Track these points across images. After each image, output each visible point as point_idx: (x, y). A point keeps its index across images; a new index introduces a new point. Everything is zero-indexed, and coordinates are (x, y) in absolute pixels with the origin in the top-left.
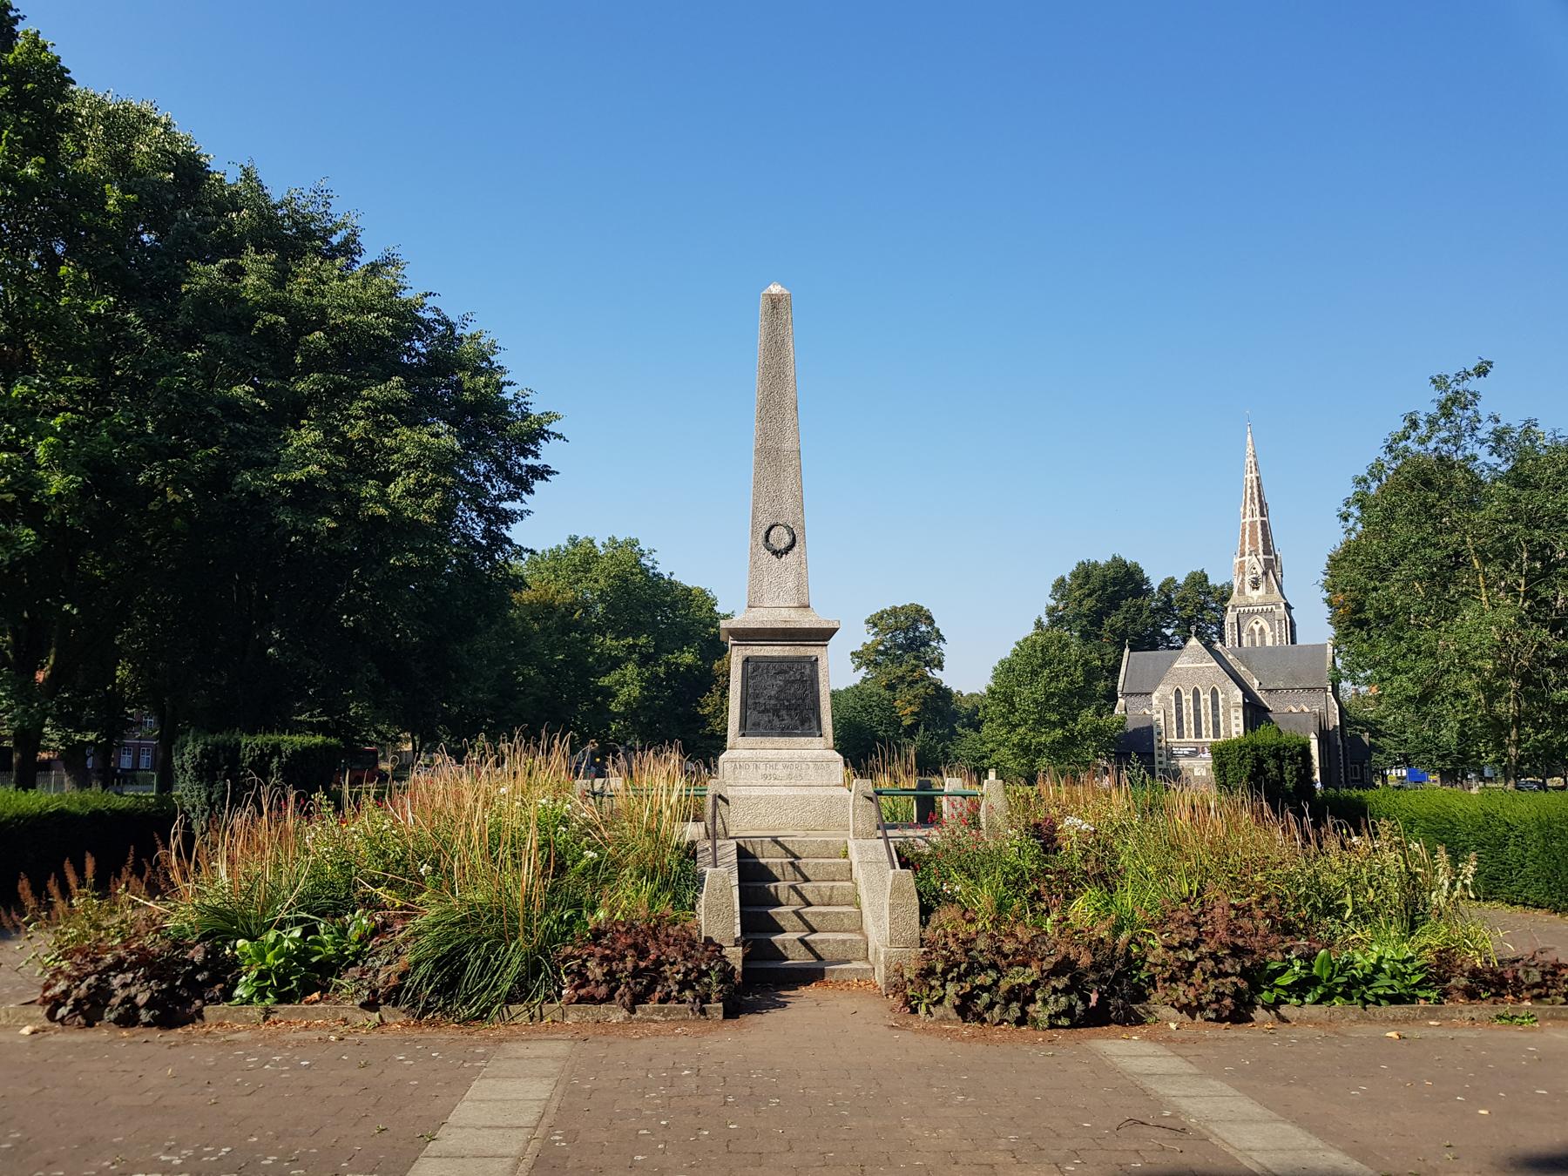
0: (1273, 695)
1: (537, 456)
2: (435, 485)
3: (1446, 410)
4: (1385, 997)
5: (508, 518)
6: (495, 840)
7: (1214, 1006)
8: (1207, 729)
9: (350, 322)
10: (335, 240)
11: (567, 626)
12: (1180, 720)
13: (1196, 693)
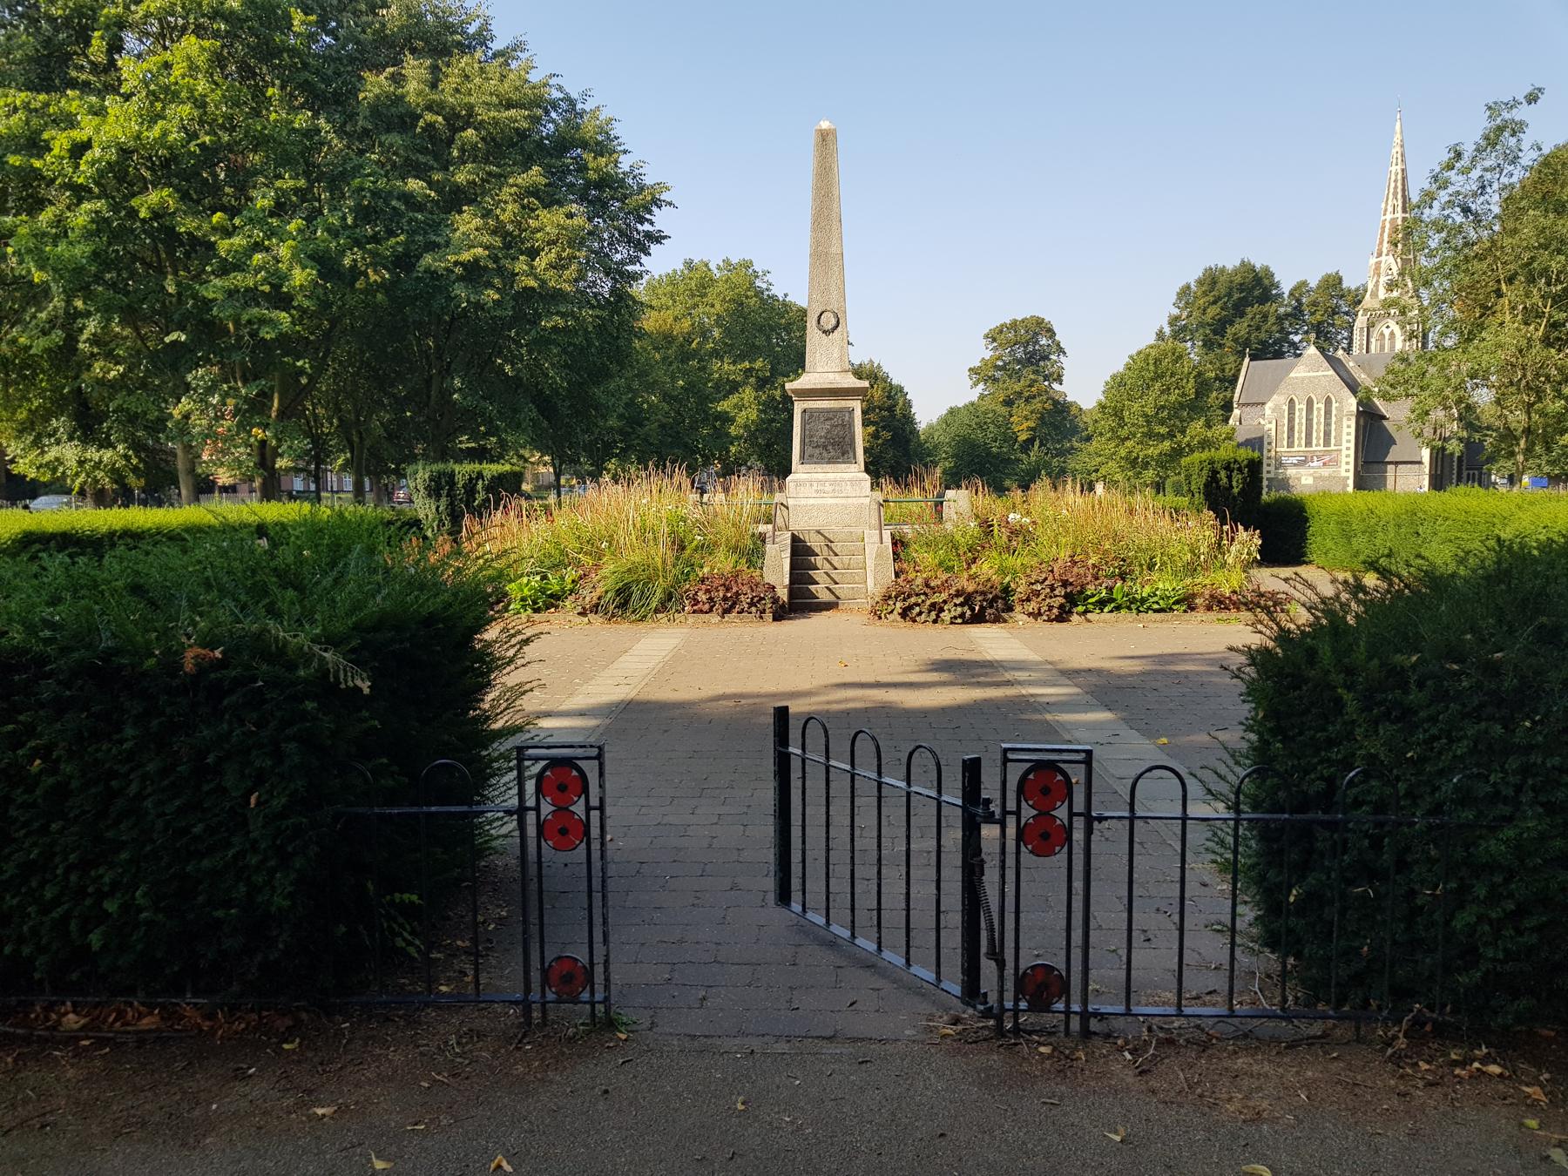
1: (652, 223)
2: (572, 257)
3: (1491, 140)
6: (643, 530)
8: (1318, 438)
10: (472, 30)
11: (685, 356)
12: (1291, 429)
13: (1310, 403)
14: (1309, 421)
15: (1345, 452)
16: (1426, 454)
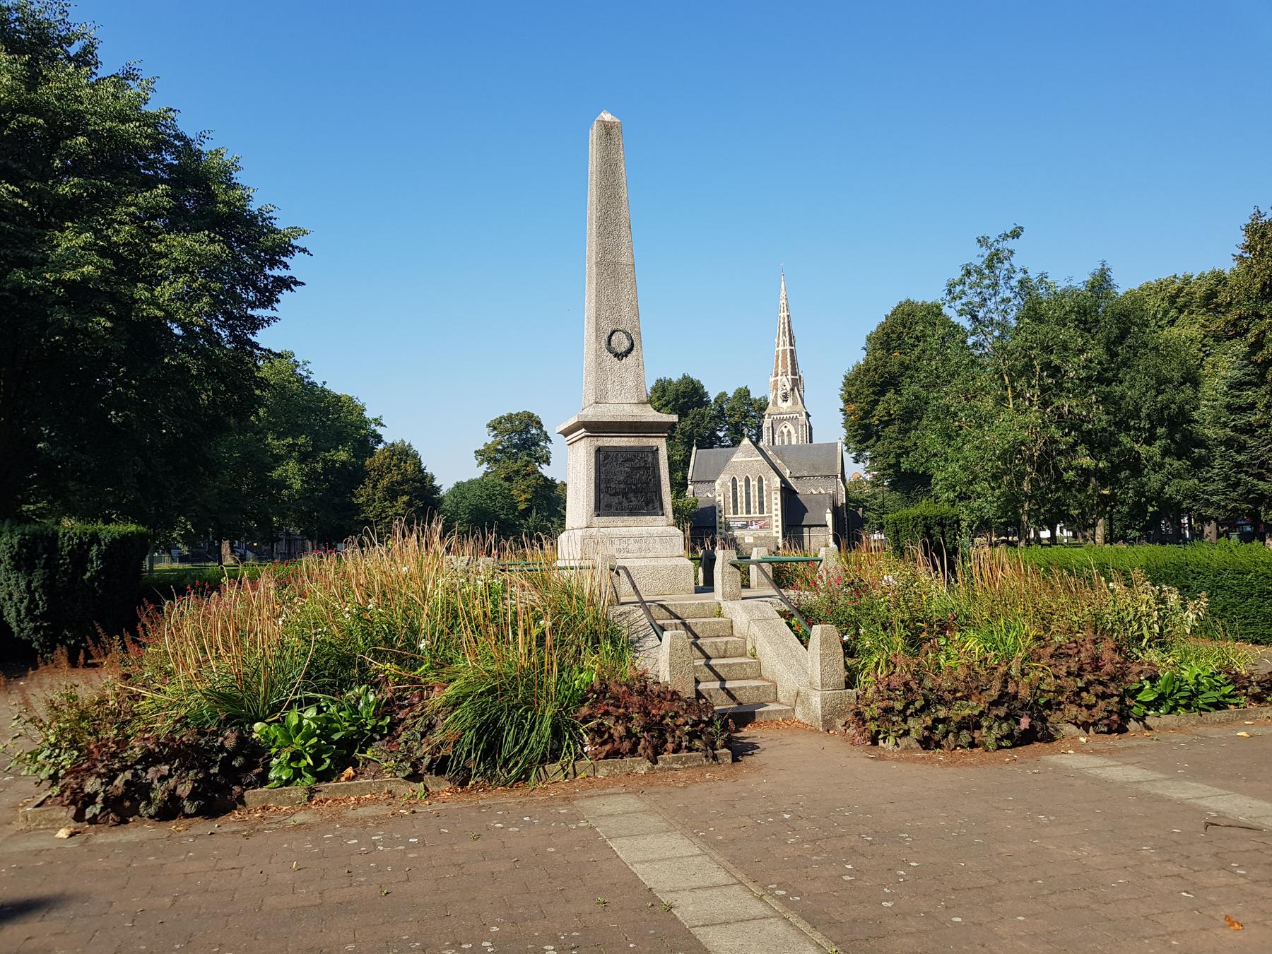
0: (800, 481)
1: (286, 267)
4: (1210, 705)
5: (256, 324)
7: (1106, 722)
9: (110, 130)
12: (735, 501)
14: (748, 494)
15: (774, 518)
16: (829, 518)
